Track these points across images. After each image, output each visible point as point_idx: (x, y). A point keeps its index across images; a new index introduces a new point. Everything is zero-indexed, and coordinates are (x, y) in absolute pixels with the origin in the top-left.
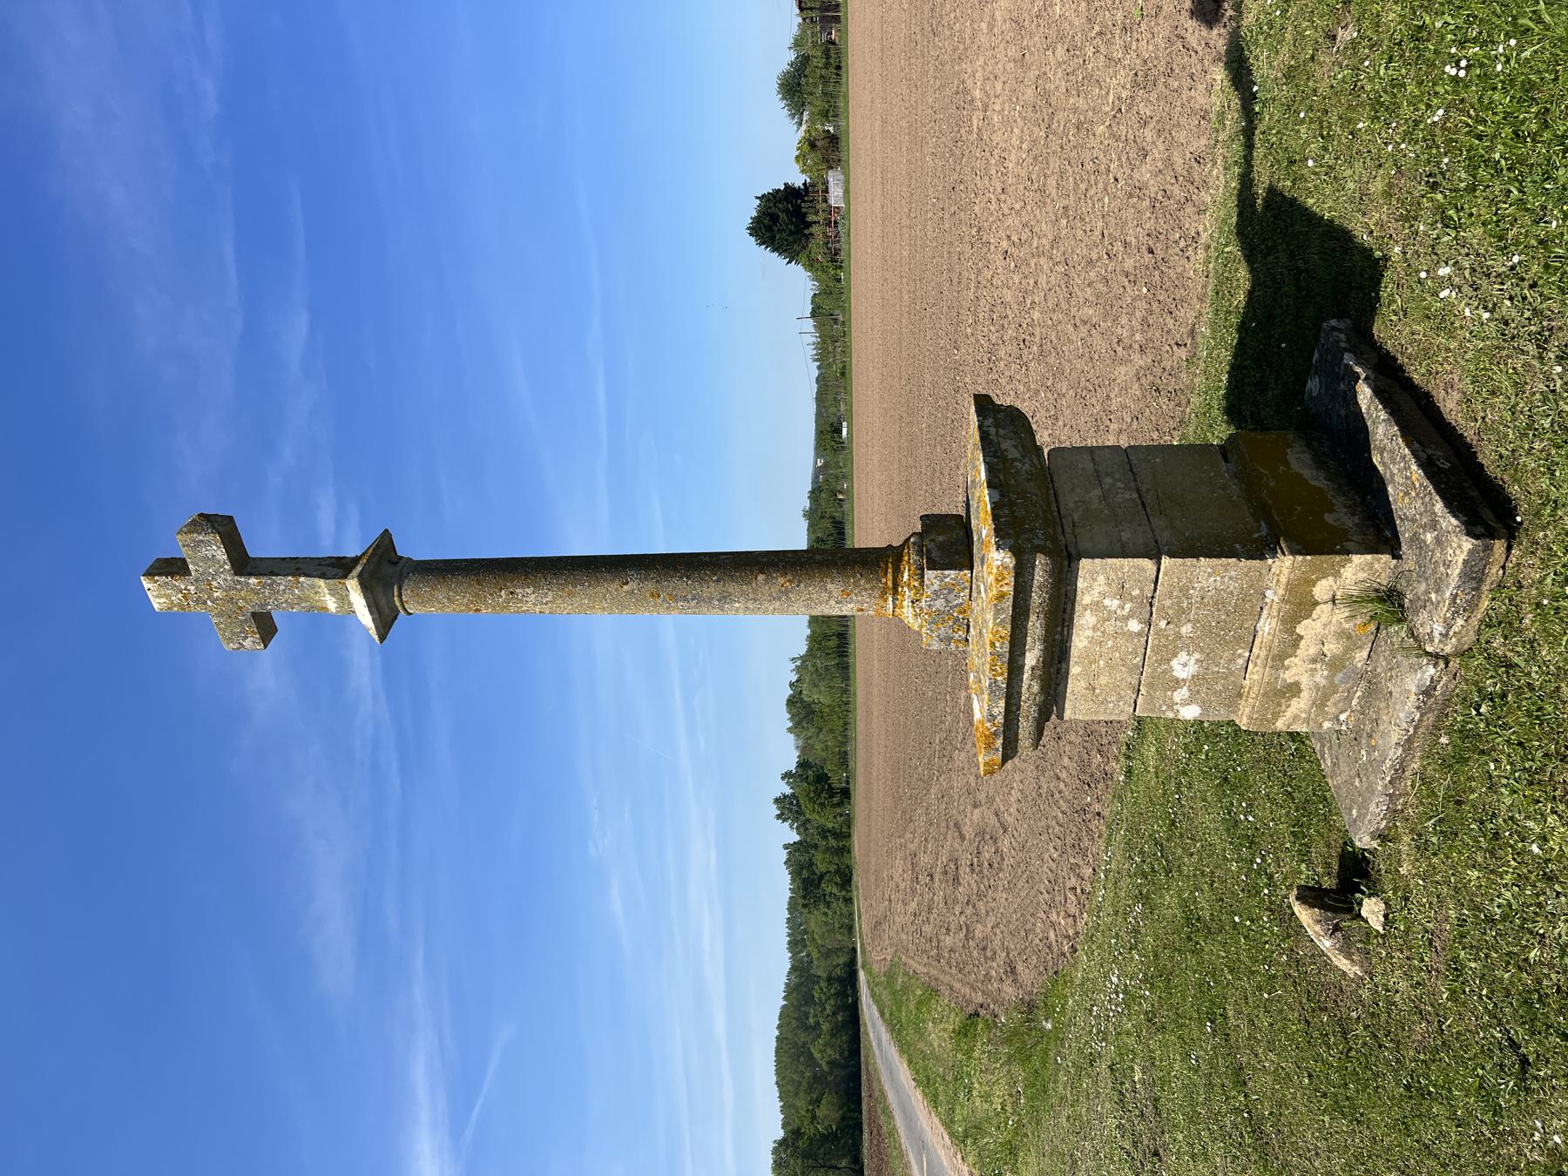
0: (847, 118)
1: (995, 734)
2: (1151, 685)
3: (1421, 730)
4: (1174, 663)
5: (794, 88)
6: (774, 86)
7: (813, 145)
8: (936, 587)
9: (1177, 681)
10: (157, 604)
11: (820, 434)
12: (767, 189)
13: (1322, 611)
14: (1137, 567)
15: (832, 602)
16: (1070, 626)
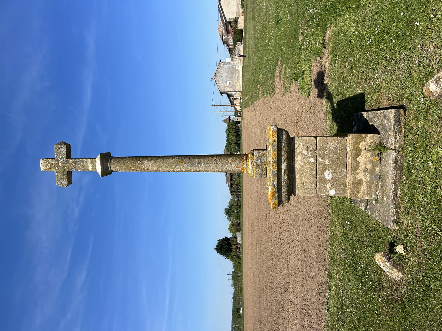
0: (242, 218)
1: (275, 191)
2: (320, 182)
3: (398, 177)
4: (325, 174)
5: (229, 212)
6: (224, 211)
7: (233, 225)
8: (257, 156)
9: (327, 180)
10: (42, 168)
11: (233, 312)
12: (221, 238)
13: (363, 152)
14: (310, 140)
15: (229, 164)
16: (294, 161)
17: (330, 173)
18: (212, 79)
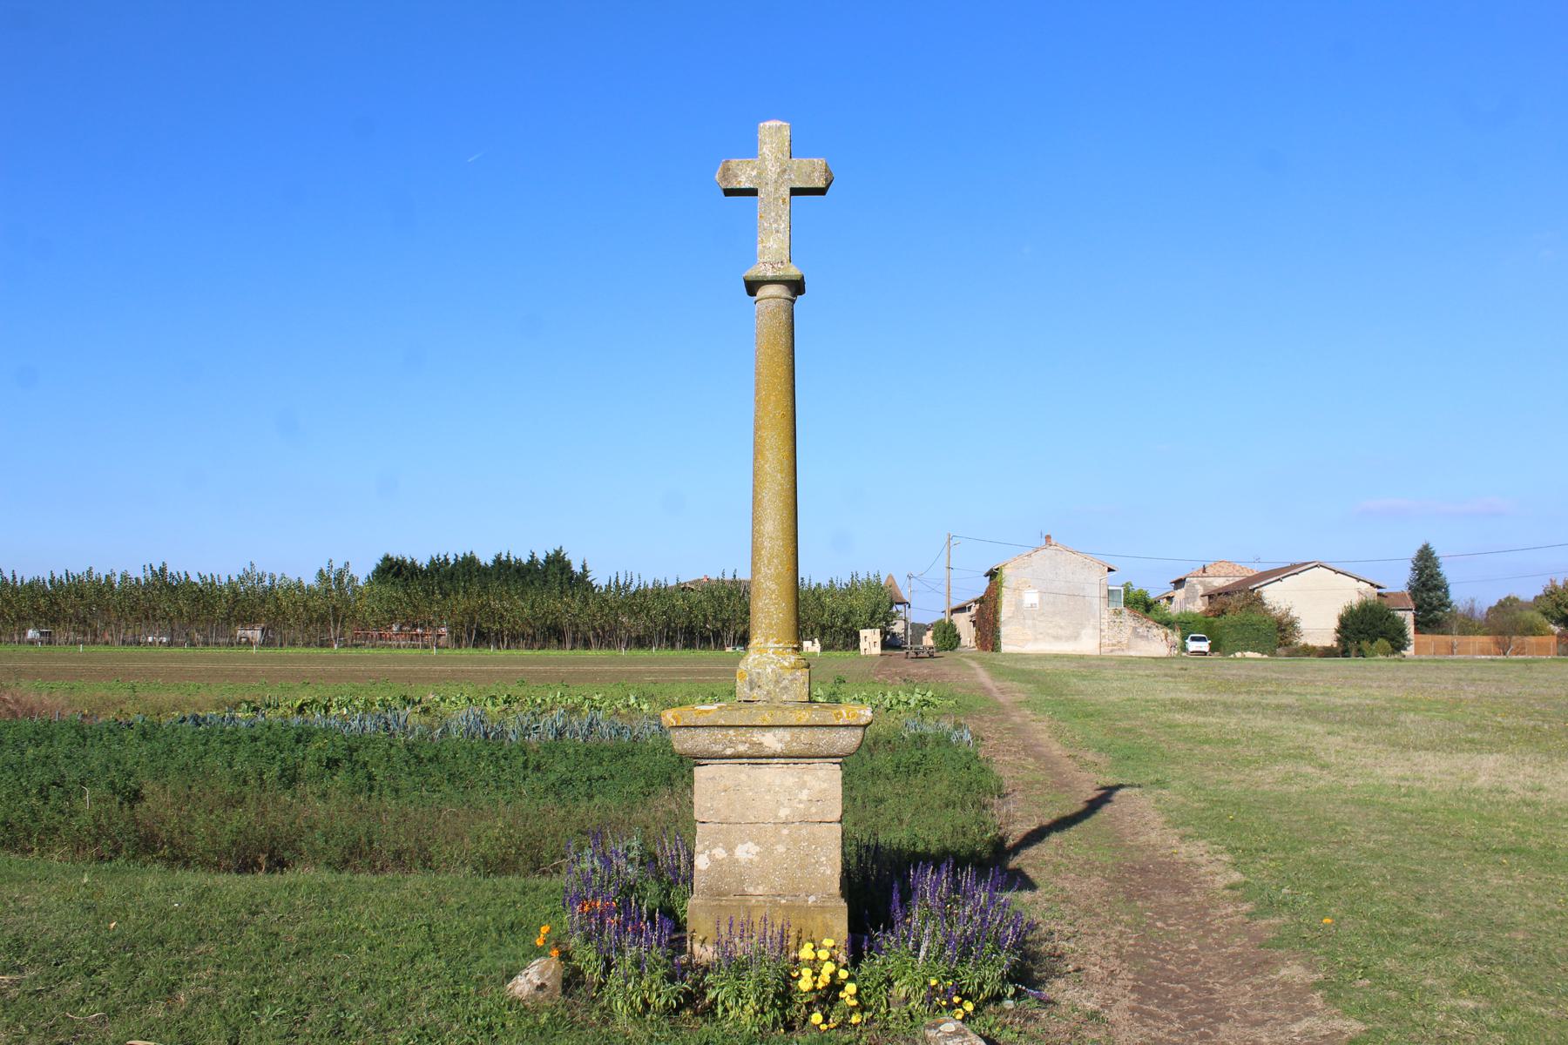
18: (1048, 537)
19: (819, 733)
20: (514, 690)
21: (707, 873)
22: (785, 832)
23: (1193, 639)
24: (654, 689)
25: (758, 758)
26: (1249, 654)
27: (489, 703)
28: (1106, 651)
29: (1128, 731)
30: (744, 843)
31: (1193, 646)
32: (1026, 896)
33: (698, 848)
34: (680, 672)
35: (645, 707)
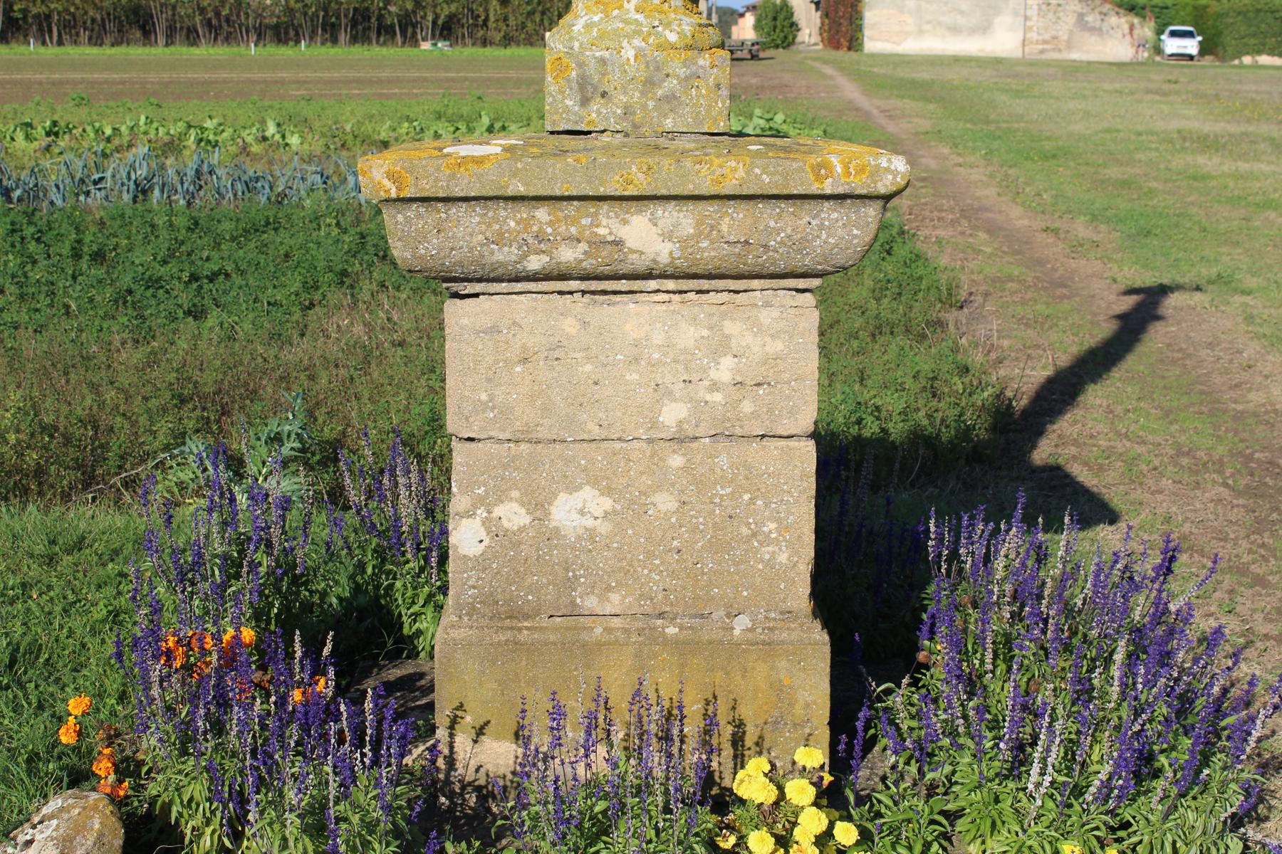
4: (588, 493)
17: (590, 523)
19: (768, 214)
20: (65, 114)
21: (481, 563)
22: (676, 461)
23: (1174, 34)
24: (308, 111)
25: (610, 277)
26: (1264, 59)
27: (20, 136)
28: (1033, 51)
29: (1125, 184)
30: (573, 488)
31: (1172, 45)
32: (1107, 536)
33: (459, 502)
34: (348, 82)
35: (294, 140)
